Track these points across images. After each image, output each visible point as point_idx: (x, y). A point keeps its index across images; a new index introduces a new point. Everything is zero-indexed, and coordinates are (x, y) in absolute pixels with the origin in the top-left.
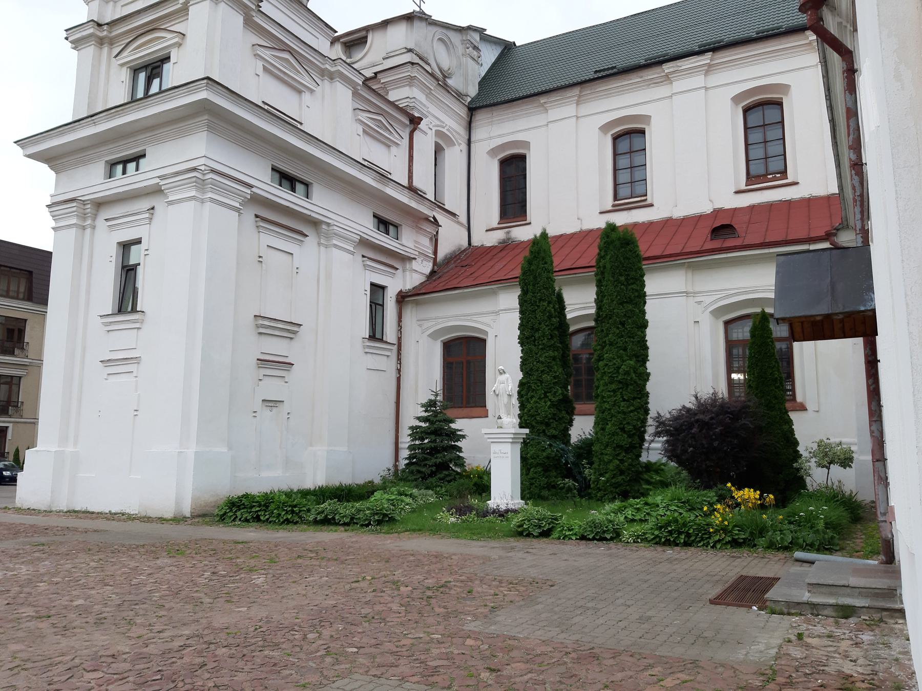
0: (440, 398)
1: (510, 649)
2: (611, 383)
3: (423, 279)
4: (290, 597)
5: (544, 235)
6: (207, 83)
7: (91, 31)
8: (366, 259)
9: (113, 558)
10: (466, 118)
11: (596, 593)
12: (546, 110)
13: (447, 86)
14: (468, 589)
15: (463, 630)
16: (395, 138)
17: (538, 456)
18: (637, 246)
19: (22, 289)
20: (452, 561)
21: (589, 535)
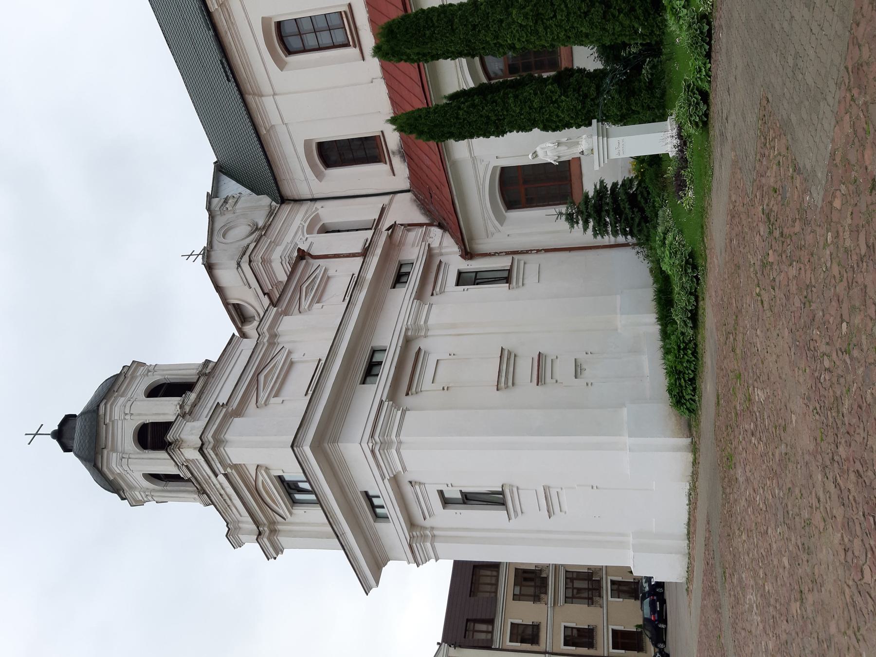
0: (563, 209)
1: (846, 162)
2: (537, 32)
3: (447, 235)
4: (780, 371)
5: (393, 121)
6: (297, 446)
7: (265, 540)
8: (434, 292)
9: (737, 518)
10: (291, 205)
11: (776, 52)
12: (273, 126)
13: (265, 226)
14: (772, 193)
15: (822, 207)
16: (320, 273)
17: (619, 103)
18: (394, 20)
19: (489, 573)
20: (738, 201)
21: (705, 50)
